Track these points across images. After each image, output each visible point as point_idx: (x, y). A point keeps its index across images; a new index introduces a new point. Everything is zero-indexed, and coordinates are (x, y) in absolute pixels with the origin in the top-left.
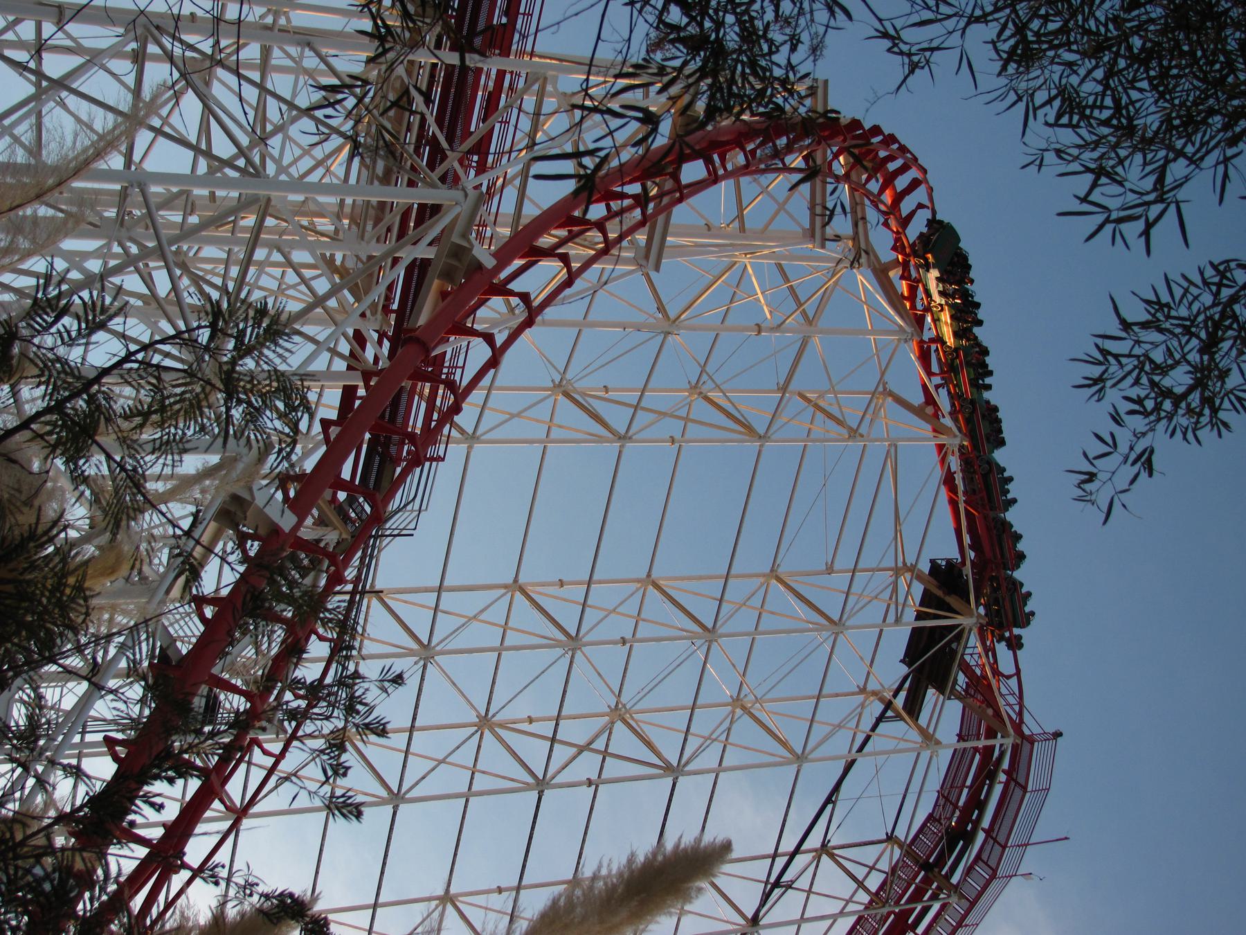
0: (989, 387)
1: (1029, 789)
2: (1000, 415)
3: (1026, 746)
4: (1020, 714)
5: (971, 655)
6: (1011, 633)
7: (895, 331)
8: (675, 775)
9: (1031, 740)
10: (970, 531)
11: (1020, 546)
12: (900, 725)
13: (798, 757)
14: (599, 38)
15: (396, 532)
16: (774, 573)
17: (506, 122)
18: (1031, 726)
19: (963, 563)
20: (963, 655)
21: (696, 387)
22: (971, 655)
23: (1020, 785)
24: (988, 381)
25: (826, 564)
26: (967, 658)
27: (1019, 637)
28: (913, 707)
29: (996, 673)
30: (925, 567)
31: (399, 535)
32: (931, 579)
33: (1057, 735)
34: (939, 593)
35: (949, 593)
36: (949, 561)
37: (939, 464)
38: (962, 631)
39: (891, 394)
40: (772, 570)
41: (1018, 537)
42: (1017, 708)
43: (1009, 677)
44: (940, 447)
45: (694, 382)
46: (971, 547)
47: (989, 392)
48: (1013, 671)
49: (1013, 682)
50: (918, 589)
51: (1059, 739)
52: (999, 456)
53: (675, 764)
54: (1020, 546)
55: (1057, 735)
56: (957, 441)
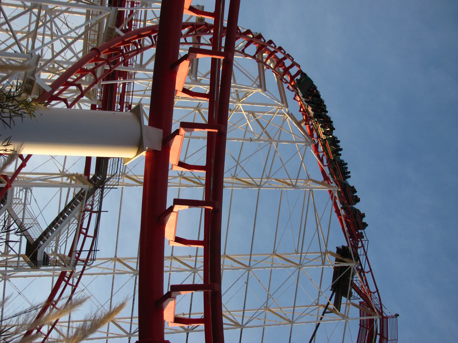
0: (340, 155)
1: (389, 339)
2: (325, 103)
3: (385, 320)
4: (381, 308)
5: (356, 281)
6: (358, 232)
7: (304, 142)
8: (242, 327)
9: (387, 318)
10: (347, 226)
11: (364, 220)
12: (333, 315)
13: (291, 322)
14: (247, 284)
15: (111, 187)
16: (274, 253)
17: (136, 25)
18: (387, 312)
19: (348, 245)
20: (352, 281)
21: (234, 176)
22: (356, 281)
23: (385, 338)
24: (340, 152)
25: (295, 250)
26: (355, 282)
27: (362, 233)
28: (338, 304)
29: (370, 292)
30: (335, 251)
31: (112, 188)
32: (337, 254)
33: (397, 315)
34: (341, 258)
35: (345, 257)
36: (343, 247)
37: (330, 198)
38: (350, 268)
39: (311, 180)
40: (274, 252)
41: (363, 216)
42: (379, 306)
43: (374, 293)
44: (330, 191)
45: (233, 175)
46: (349, 237)
47: (341, 151)
48: (375, 290)
49: (376, 294)
50: (334, 258)
51: (398, 317)
52: (357, 206)
53: (241, 323)
54: (364, 220)
55: (397, 315)
56: (336, 189)
